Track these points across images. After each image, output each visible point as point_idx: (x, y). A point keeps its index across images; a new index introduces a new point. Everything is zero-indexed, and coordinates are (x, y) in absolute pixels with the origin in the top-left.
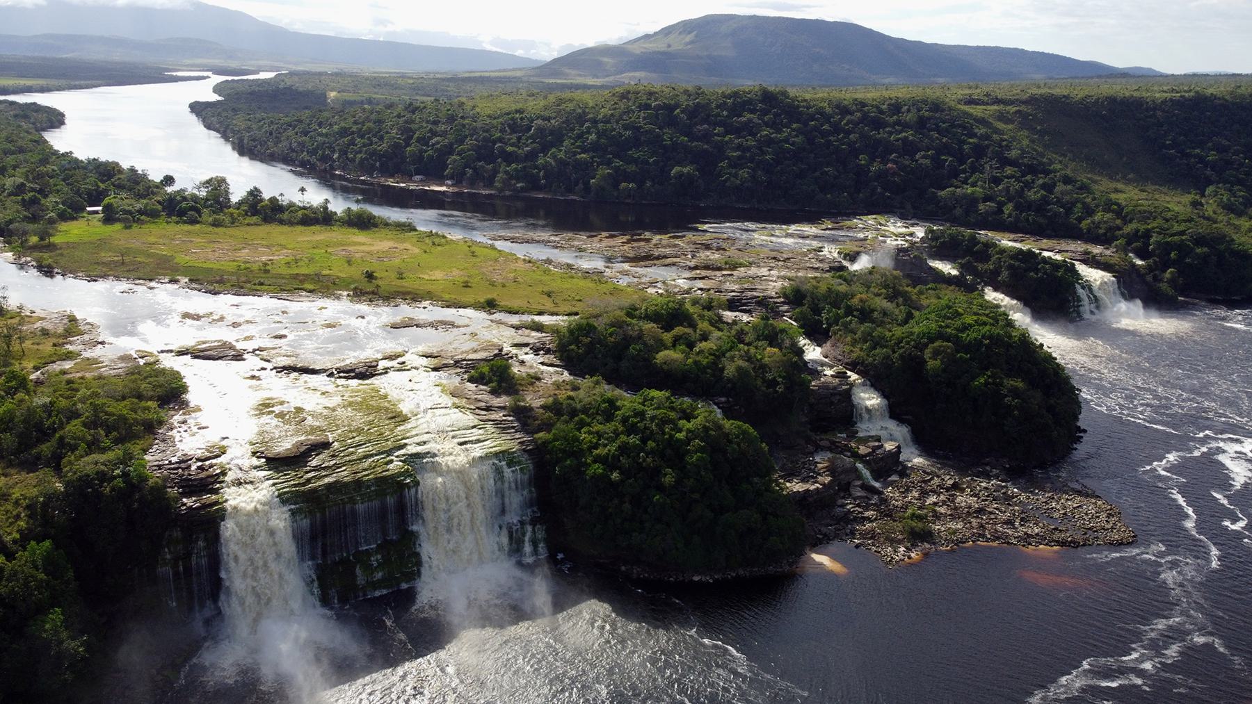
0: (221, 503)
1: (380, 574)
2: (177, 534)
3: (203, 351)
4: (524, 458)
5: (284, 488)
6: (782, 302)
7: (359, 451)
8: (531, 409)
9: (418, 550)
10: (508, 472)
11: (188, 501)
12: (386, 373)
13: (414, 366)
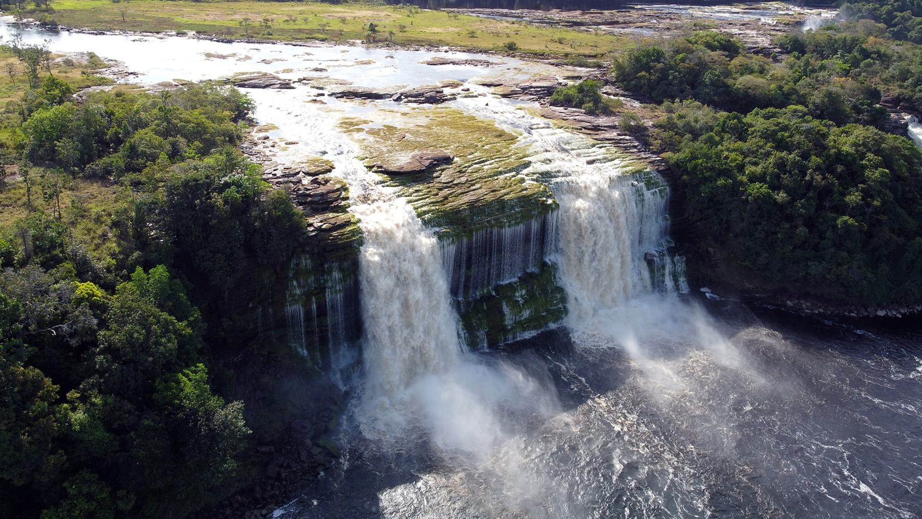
0: (355, 223)
1: (528, 312)
2: (306, 262)
3: (245, 81)
4: (660, 179)
5: (422, 206)
6: (779, 52)
7: (486, 167)
8: (646, 129)
9: (559, 284)
10: (648, 194)
11: (316, 221)
12: (455, 99)
13: (480, 93)
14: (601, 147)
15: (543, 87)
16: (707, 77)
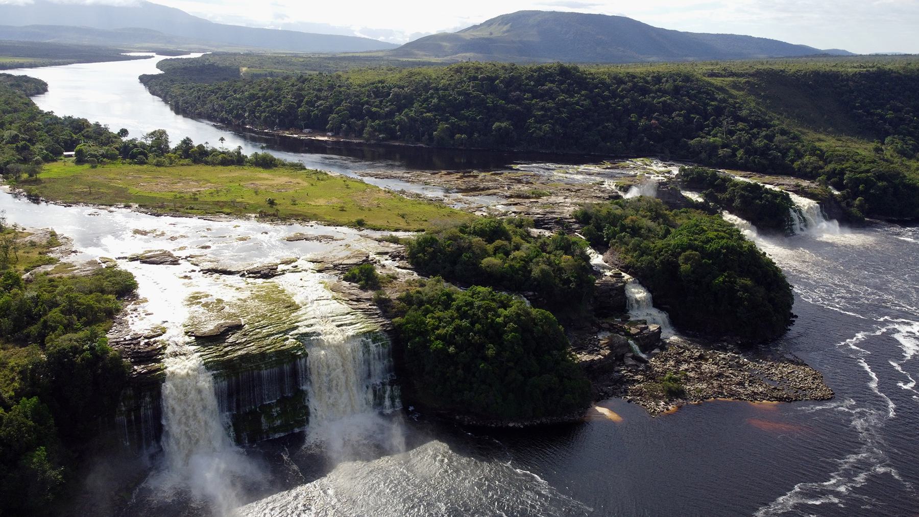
0: (162, 370)
1: (279, 421)
2: (130, 392)
3: (149, 258)
4: (385, 336)
5: (208, 358)
7: (264, 331)
9: (307, 404)
10: (373, 347)
11: (138, 368)
12: (284, 274)
13: (304, 268)
14: (353, 315)
15: (347, 264)
16: (465, 256)
